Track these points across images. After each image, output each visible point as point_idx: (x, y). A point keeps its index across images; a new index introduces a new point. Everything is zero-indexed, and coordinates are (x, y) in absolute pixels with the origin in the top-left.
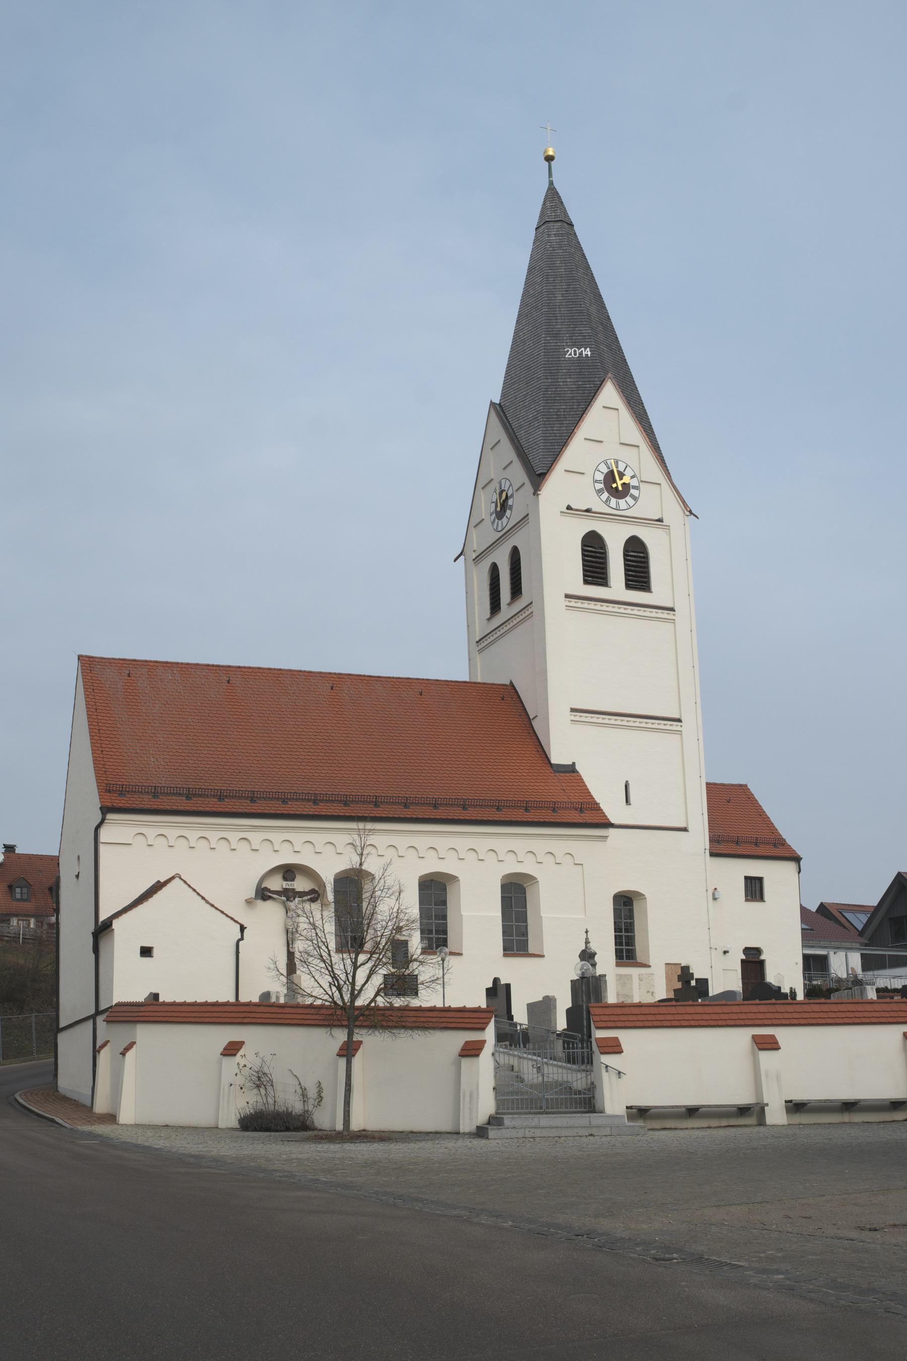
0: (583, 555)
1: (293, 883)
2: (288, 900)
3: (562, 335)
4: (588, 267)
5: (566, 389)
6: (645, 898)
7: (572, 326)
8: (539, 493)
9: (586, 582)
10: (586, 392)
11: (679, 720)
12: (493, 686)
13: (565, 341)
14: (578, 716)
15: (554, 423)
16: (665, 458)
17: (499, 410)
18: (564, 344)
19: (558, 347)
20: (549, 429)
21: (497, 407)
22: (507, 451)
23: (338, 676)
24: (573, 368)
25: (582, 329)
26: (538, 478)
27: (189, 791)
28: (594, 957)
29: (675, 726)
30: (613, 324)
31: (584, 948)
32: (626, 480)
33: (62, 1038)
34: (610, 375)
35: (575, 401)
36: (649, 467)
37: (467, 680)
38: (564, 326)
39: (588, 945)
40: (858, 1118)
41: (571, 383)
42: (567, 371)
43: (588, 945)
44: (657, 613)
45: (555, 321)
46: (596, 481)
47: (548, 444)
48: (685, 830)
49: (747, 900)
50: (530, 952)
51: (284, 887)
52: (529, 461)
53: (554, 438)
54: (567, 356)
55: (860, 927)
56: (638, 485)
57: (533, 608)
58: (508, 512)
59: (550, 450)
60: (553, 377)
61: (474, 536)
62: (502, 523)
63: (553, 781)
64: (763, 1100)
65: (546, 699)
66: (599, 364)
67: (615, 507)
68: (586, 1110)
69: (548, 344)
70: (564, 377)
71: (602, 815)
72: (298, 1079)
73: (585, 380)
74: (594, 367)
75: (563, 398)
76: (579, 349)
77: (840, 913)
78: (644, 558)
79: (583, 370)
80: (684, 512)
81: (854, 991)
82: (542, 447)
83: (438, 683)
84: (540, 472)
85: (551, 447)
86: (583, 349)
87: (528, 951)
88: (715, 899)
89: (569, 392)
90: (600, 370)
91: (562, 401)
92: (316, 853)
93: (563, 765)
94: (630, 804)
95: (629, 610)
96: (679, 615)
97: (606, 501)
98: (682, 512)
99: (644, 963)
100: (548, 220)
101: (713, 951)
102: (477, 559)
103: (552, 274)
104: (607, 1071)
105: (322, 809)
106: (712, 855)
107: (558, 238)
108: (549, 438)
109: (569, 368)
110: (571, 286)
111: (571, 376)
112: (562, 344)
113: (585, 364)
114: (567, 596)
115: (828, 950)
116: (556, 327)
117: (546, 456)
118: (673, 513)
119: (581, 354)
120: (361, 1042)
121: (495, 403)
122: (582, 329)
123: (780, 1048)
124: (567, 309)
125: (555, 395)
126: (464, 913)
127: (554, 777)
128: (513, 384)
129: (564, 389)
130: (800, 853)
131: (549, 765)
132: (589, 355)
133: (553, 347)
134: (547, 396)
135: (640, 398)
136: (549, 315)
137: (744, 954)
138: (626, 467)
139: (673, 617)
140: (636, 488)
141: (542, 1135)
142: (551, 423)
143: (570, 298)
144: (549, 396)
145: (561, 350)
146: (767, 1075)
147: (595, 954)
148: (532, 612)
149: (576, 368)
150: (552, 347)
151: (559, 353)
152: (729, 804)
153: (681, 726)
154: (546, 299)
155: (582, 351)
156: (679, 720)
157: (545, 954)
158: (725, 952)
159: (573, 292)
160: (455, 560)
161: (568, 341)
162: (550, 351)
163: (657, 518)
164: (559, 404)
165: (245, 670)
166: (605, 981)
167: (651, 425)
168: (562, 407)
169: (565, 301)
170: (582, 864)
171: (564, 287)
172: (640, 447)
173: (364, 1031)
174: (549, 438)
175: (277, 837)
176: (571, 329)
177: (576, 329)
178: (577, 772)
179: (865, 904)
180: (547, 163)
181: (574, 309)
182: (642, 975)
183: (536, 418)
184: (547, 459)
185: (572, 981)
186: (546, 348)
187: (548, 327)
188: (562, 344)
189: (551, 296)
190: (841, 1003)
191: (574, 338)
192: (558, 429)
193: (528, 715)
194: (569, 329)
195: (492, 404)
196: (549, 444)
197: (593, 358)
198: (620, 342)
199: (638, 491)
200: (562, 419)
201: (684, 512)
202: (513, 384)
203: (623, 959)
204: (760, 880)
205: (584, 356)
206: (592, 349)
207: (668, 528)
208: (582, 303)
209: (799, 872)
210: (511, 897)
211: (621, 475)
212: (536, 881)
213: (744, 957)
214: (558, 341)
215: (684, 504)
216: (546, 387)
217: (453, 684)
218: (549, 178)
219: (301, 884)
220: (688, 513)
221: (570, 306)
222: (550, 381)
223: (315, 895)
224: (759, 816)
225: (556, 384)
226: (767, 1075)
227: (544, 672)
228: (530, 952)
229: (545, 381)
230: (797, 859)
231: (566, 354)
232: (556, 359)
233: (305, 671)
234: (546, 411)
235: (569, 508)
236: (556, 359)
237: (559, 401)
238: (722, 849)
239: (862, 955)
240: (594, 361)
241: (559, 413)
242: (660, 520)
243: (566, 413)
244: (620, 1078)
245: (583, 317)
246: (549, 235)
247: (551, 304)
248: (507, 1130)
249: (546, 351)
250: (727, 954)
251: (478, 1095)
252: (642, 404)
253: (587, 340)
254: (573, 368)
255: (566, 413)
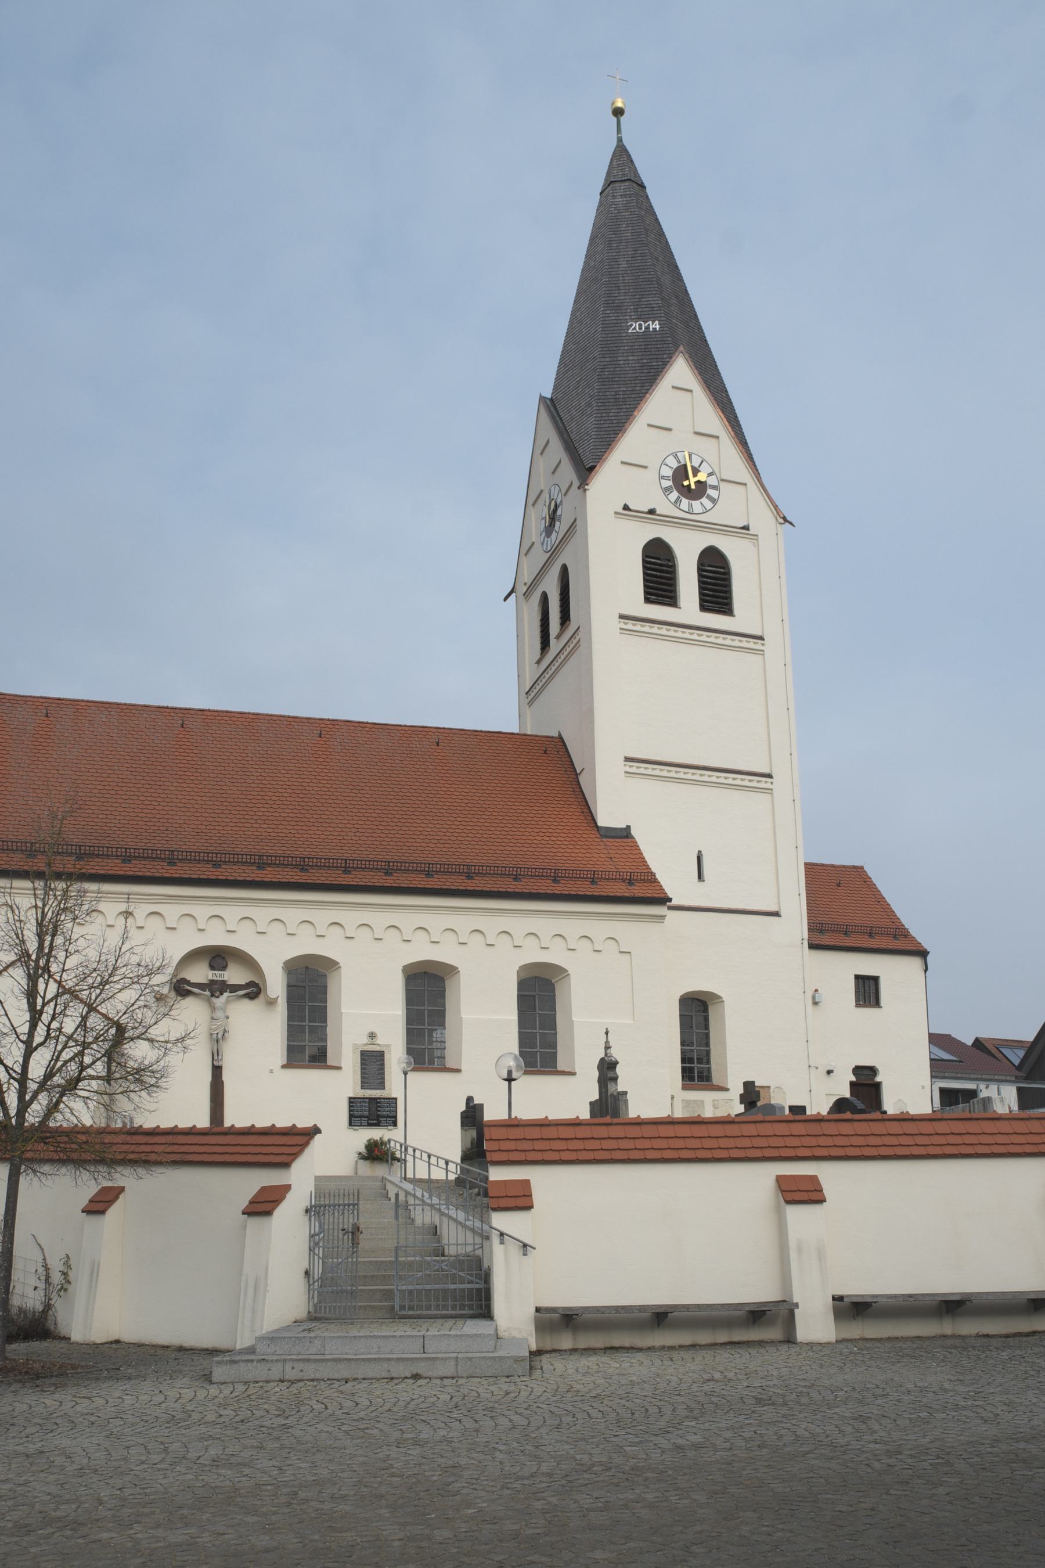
0: (644, 567)
1: (222, 972)
2: (212, 995)
3: (625, 308)
4: (661, 234)
5: (627, 369)
6: (723, 1001)
7: (637, 297)
8: (586, 487)
9: (647, 600)
10: (653, 370)
11: (770, 776)
12: (535, 738)
13: (628, 314)
14: (634, 767)
15: (610, 407)
16: (754, 456)
17: (551, 406)
18: (628, 317)
19: (619, 322)
20: (604, 415)
21: (548, 401)
22: (557, 451)
23: (332, 723)
24: (636, 344)
25: (650, 299)
26: (586, 471)
27: (80, 850)
28: (615, 1067)
29: (764, 783)
30: (692, 299)
31: (603, 1056)
32: (702, 477)
33: (432, 1177)
34: (681, 348)
35: (638, 382)
36: (733, 464)
37: (517, 731)
38: (628, 297)
39: (608, 1052)
40: (968, 1327)
41: (634, 362)
42: (629, 348)
43: (608, 1052)
44: (740, 641)
45: (617, 292)
46: (663, 477)
47: (601, 433)
48: (777, 914)
49: (858, 1005)
50: (559, 1068)
51: (210, 978)
52: (579, 455)
53: (610, 425)
54: (630, 331)
55: (1017, 1062)
56: (717, 484)
57: (581, 635)
58: (557, 524)
59: (604, 440)
60: (611, 355)
61: (525, 565)
62: (551, 541)
63: (599, 847)
64: (791, 1296)
65: (593, 745)
66: (669, 339)
67: (687, 510)
68: (471, 1312)
69: (607, 319)
70: (625, 354)
71: (659, 888)
72: (42, 1250)
73: (652, 357)
74: (663, 342)
75: (623, 379)
76: (645, 322)
77: (997, 1048)
78: (725, 574)
79: (649, 346)
80: (777, 519)
81: (974, 1104)
82: (594, 437)
83: (463, 732)
84: (590, 465)
85: (605, 436)
86: (650, 322)
87: (556, 1068)
88: (815, 1003)
89: (631, 372)
90: (671, 345)
91: (622, 383)
92: (258, 933)
93: (613, 828)
94: (704, 881)
95: (705, 636)
96: (768, 646)
97: (676, 502)
98: (774, 520)
99: (721, 1085)
100: (613, 180)
101: (813, 1070)
102: (527, 594)
103: (616, 239)
104: (502, 1242)
105: (269, 874)
106: (812, 946)
107: (625, 199)
108: (603, 426)
109: (632, 344)
110: (639, 252)
111: (635, 354)
112: (624, 318)
113: (651, 340)
114: (622, 617)
115: (978, 1082)
116: (618, 298)
117: (599, 447)
118: (763, 520)
119: (647, 328)
120: (122, 1189)
121: (544, 398)
122: (650, 299)
123: (825, 1201)
124: (632, 278)
125: (613, 376)
126: (465, 1015)
127: (601, 843)
128: (567, 372)
129: (624, 369)
130: (926, 946)
131: (595, 829)
132: (658, 329)
133: (613, 322)
134: (603, 377)
135: (724, 385)
136: (610, 285)
137: (854, 1074)
138: (702, 462)
139: (762, 648)
140: (716, 488)
141: (318, 1376)
142: (607, 408)
143: (636, 265)
144: (606, 377)
145: (622, 325)
146: (800, 1250)
147: (616, 1063)
148: (579, 641)
149: (640, 344)
150: (611, 322)
151: (620, 328)
152: (840, 888)
153: (772, 783)
154: (607, 267)
155: (649, 325)
156: (770, 776)
157: (577, 1070)
158: (829, 1072)
159: (641, 258)
160: (505, 599)
161: (633, 314)
162: (609, 325)
163: (742, 526)
164: (618, 386)
165: (209, 713)
166: (626, 1101)
167: (728, 395)
168: (622, 389)
169: (631, 268)
170: (630, 953)
171: (629, 253)
172: (720, 438)
173: (127, 1171)
174: (603, 426)
175: (201, 911)
176: (637, 300)
177: (643, 300)
178: (632, 837)
179: (1023, 1040)
180: (615, 119)
181: (641, 277)
182: (718, 1100)
183: (589, 405)
184: (599, 450)
185: (591, 1103)
186: (604, 322)
187: (608, 299)
188: (624, 318)
189: (614, 263)
190: (940, 1120)
191: (640, 310)
192: (615, 414)
193: (574, 768)
194: (634, 300)
195: (542, 399)
196: (604, 433)
197: (662, 332)
198: (700, 321)
199: (717, 492)
200: (621, 403)
201: (777, 519)
202: (567, 372)
203: (694, 1080)
204: (875, 980)
205: (651, 329)
206: (662, 322)
207: (755, 538)
208: (651, 270)
209: (926, 970)
210: (534, 996)
211: (696, 471)
212: (567, 974)
213: (854, 1079)
214: (620, 315)
215: (776, 509)
216: (602, 367)
217: (483, 734)
218: (618, 134)
219: (234, 975)
220: (782, 521)
221: (636, 274)
222: (608, 359)
223: (254, 991)
224: (876, 903)
225: (615, 363)
226: (800, 1250)
227: (591, 710)
228: (559, 1068)
229: (603, 360)
230: (923, 954)
231: (629, 329)
232: (617, 335)
233: (289, 717)
234: (601, 394)
235: (626, 508)
236: (617, 335)
237: (618, 383)
238: (826, 939)
239: (1019, 1089)
240: (664, 335)
241: (617, 397)
242: (746, 528)
243: (626, 396)
244: (525, 1254)
245: (652, 286)
246: (614, 197)
247: (613, 273)
248: (249, 1364)
249: (604, 326)
250: (831, 1074)
251: (266, 1285)
252: (726, 391)
253: (655, 312)
254: (636, 344)
255: (626, 396)
